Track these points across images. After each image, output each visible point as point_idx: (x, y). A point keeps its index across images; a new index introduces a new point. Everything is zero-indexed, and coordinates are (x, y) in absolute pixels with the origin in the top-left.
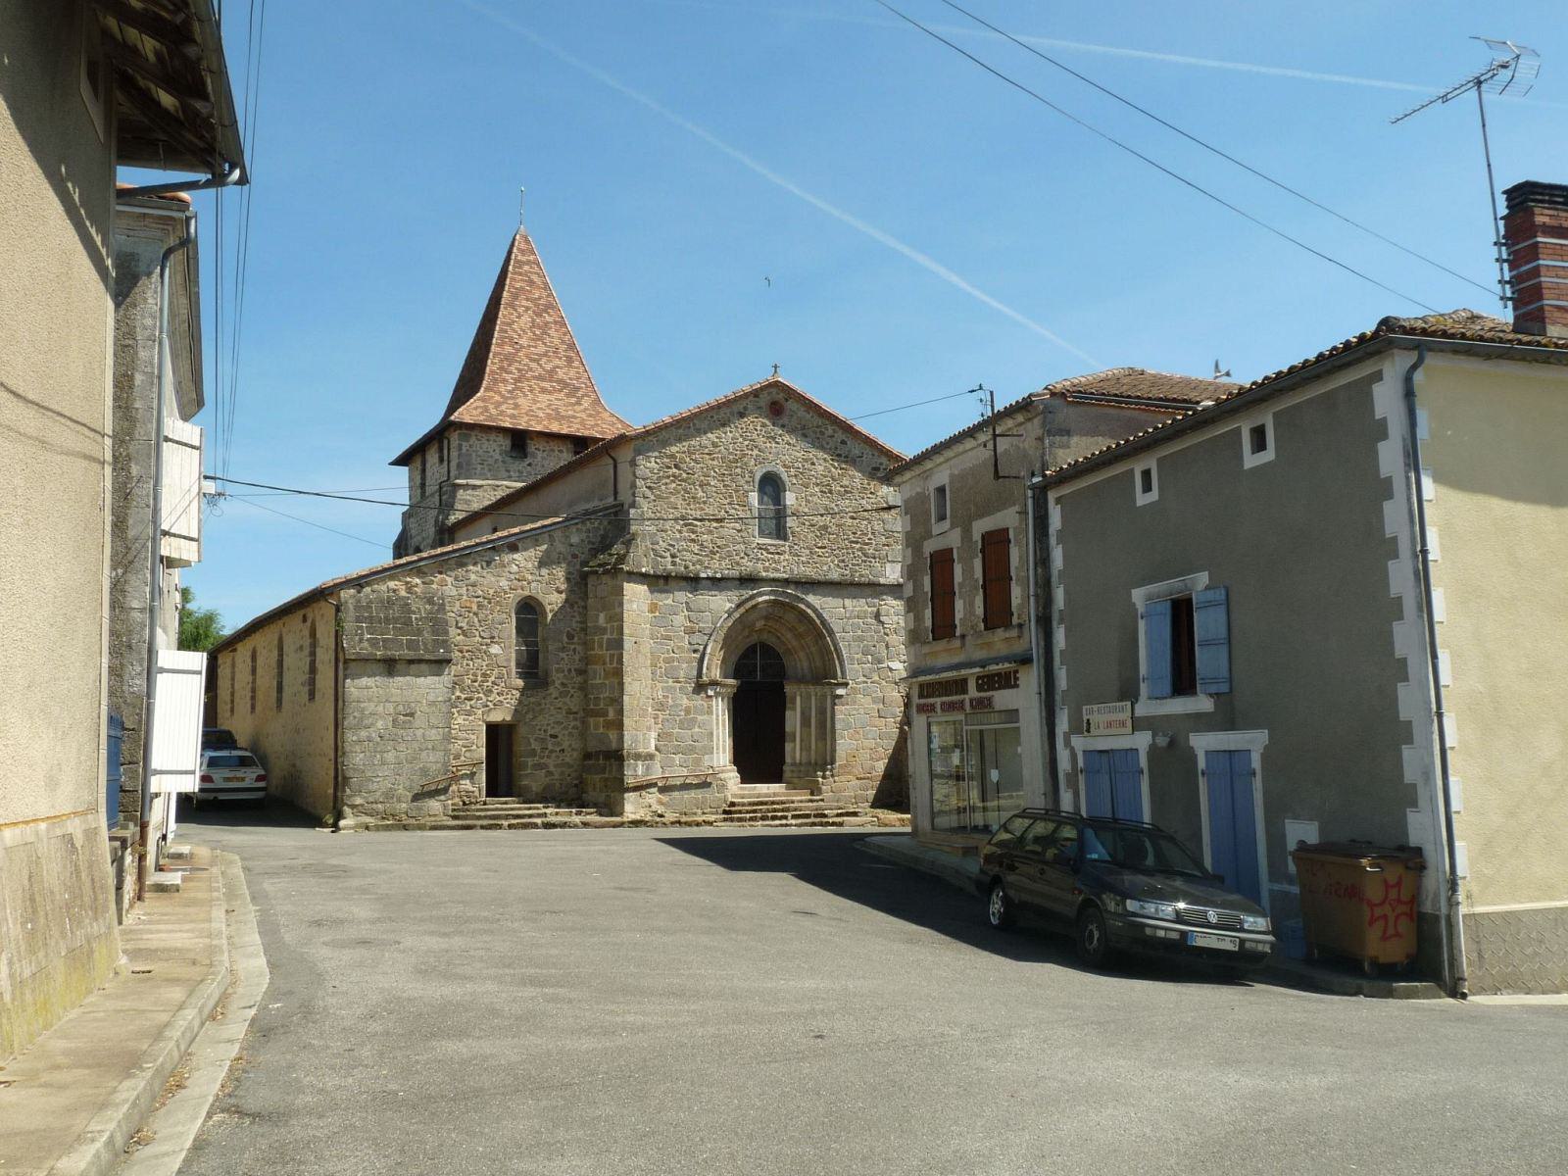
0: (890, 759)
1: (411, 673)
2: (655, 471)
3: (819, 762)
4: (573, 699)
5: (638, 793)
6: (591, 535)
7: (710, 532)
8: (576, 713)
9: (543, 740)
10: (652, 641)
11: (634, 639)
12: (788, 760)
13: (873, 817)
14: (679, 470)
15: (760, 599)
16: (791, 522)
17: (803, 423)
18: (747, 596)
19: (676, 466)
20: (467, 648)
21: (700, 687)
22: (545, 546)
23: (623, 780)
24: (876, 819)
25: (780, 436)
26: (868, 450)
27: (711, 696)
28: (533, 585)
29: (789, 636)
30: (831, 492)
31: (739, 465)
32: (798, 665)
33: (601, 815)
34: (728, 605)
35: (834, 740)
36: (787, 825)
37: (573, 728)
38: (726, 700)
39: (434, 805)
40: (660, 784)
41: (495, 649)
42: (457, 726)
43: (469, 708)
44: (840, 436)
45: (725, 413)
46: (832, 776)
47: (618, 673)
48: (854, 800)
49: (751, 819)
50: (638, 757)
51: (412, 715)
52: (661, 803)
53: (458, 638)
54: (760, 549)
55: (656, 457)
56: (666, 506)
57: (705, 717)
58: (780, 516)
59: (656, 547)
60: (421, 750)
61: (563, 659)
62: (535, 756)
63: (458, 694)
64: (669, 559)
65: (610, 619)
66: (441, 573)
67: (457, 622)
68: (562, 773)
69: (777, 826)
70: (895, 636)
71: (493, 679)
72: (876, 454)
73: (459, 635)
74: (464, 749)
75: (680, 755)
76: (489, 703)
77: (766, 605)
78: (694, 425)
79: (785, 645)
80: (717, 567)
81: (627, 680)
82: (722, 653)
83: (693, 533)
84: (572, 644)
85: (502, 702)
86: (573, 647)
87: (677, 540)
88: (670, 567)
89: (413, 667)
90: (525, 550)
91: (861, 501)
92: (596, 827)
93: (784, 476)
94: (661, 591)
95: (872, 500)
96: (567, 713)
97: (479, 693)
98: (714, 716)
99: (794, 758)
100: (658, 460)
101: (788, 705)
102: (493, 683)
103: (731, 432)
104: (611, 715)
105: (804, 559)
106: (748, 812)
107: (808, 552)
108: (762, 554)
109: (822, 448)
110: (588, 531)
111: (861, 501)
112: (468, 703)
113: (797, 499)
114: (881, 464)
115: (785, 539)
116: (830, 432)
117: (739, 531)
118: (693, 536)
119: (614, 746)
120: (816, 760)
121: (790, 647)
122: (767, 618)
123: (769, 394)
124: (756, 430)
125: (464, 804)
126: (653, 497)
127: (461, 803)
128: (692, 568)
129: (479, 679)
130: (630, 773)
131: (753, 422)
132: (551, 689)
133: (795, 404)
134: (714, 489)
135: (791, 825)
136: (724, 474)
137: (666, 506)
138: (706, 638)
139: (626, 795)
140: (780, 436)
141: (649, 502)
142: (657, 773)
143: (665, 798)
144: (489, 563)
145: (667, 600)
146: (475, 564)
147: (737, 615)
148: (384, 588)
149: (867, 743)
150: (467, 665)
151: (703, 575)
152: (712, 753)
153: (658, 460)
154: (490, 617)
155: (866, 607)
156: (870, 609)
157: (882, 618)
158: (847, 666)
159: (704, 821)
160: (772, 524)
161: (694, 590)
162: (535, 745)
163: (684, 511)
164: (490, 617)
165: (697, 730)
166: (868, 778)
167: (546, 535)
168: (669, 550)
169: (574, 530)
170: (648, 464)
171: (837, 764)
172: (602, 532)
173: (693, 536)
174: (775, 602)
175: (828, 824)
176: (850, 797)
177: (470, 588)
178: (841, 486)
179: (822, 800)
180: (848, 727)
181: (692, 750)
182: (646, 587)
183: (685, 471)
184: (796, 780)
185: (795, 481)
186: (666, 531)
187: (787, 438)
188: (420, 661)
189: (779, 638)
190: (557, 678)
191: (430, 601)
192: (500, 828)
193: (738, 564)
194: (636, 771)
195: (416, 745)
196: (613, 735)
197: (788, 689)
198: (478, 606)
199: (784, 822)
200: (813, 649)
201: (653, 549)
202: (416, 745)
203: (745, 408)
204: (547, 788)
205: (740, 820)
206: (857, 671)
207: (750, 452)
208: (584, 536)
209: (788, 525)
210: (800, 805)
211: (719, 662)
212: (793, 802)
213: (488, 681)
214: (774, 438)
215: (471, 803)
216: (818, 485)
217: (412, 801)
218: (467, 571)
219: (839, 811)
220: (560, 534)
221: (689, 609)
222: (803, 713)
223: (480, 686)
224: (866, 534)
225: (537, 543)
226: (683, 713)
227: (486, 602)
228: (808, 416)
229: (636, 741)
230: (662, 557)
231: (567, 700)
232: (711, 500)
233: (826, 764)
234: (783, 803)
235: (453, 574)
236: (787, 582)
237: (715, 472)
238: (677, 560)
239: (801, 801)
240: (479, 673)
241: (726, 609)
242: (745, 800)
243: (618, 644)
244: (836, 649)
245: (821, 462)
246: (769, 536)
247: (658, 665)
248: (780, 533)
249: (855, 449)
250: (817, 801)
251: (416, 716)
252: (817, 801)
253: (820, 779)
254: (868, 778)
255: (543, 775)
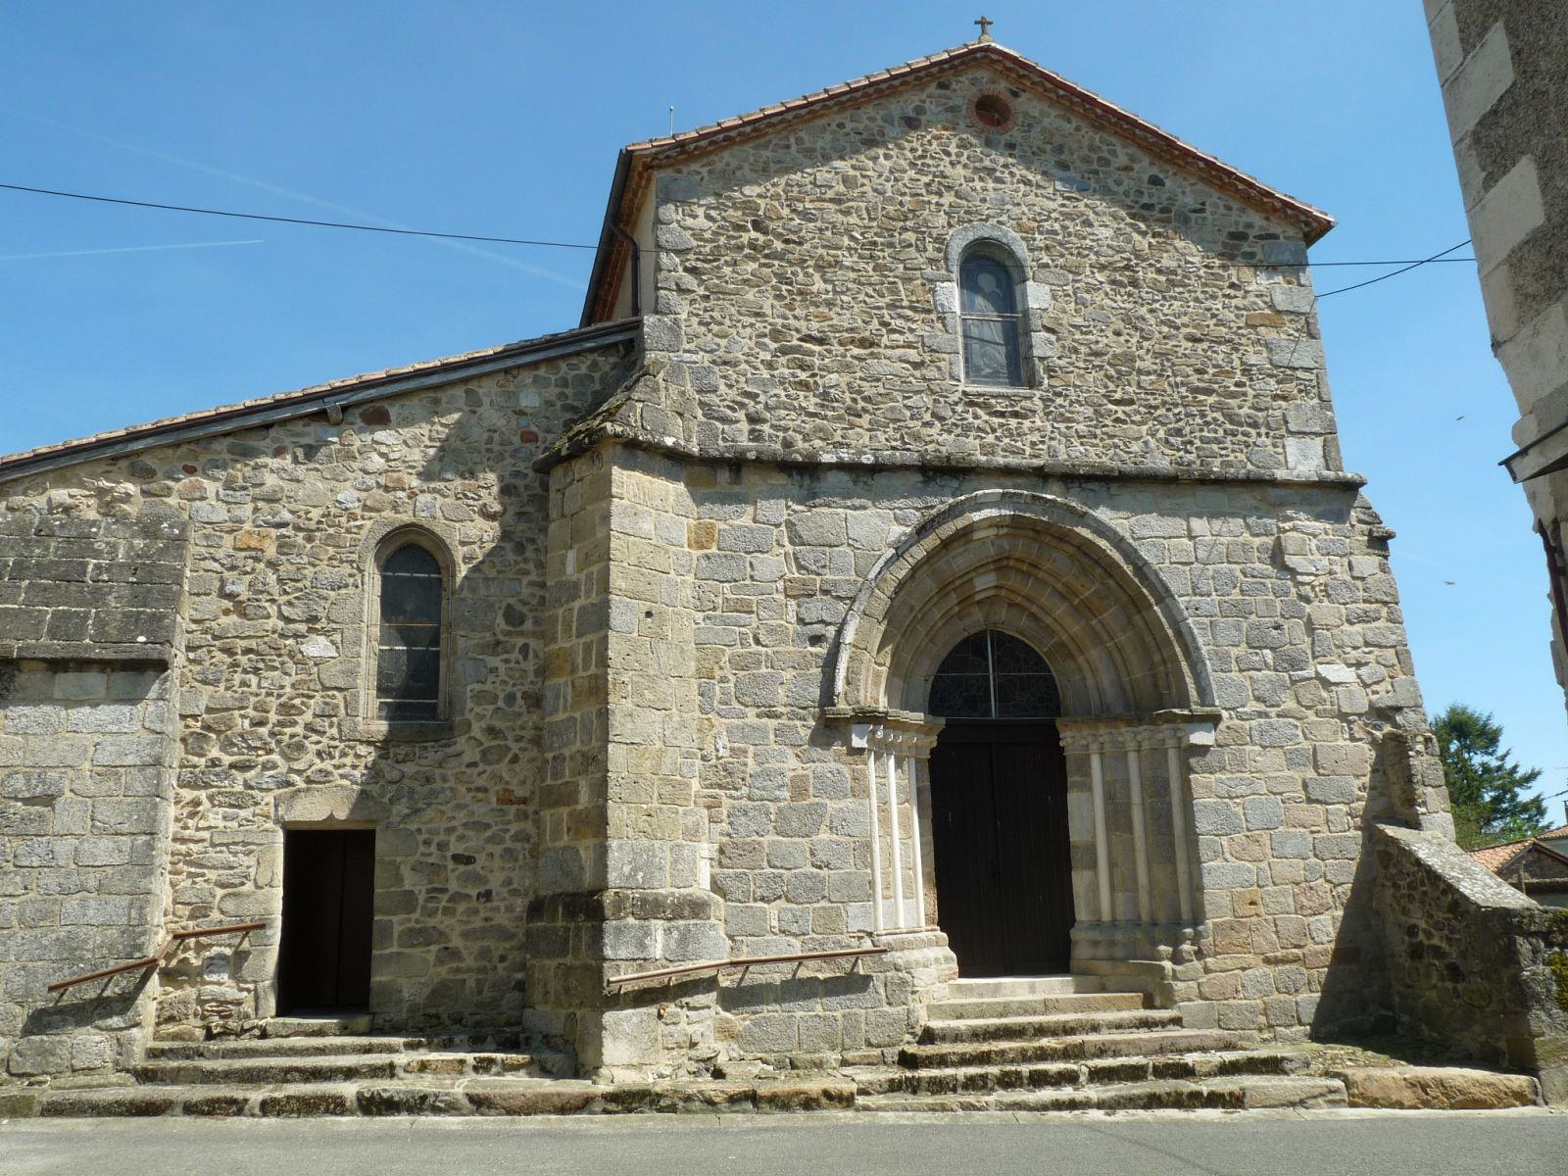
0: (1347, 908)
1: (58, 694)
2: (708, 235)
3: (1162, 918)
4: (517, 767)
5: (653, 1010)
6: (569, 391)
7: (847, 368)
8: (524, 801)
9: (435, 869)
10: (700, 616)
11: (645, 606)
12: (1082, 914)
13: (1327, 1074)
14: (765, 232)
15: (977, 516)
16: (1041, 344)
17: (1057, 140)
18: (943, 508)
19: (757, 226)
20: (244, 643)
21: (831, 728)
22: (456, 416)
23: (600, 971)
24: (1338, 1083)
25: (1006, 166)
26: (1214, 198)
27: (860, 751)
28: (423, 499)
29: (1060, 610)
30: (1134, 283)
31: (909, 224)
32: (1090, 681)
33: (546, 1072)
34: (897, 531)
35: (1195, 860)
36: (1072, 1105)
37: (516, 838)
38: (910, 766)
39: (91, 1042)
40: (725, 982)
41: (317, 647)
42: (206, 835)
43: (239, 788)
44: (1145, 167)
45: (872, 119)
46: (1200, 954)
47: (598, 690)
48: (1262, 1019)
49: (971, 1083)
50: (651, 908)
51: (49, 800)
52: (727, 1033)
53: (224, 620)
54: (972, 404)
55: (709, 207)
56: (733, 310)
57: (849, 802)
58: (1016, 332)
59: (713, 398)
60: (66, 892)
61: (494, 670)
62: (413, 911)
63: (214, 752)
64: (745, 426)
65: (585, 561)
66: (190, 471)
67: (223, 582)
68: (484, 954)
69: (1044, 1107)
70: (1326, 602)
71: (308, 717)
72: (1235, 205)
73: (226, 612)
74: (220, 892)
75: (782, 903)
76: (294, 777)
77: (992, 532)
78: (799, 141)
79: (1053, 633)
80: (865, 443)
81: (620, 705)
82: (887, 658)
83: (802, 368)
84: (522, 634)
85: (327, 773)
86: (520, 641)
87: (763, 383)
88: (744, 442)
89: (66, 681)
90: (408, 422)
91: (1208, 304)
92: (510, 1112)
93: (1021, 249)
94: (725, 499)
95: (1234, 302)
96: (500, 801)
97: (270, 752)
98: (874, 801)
99: (1096, 909)
100: (713, 213)
101: (1073, 778)
102: (309, 727)
103: (887, 157)
104: (584, 798)
105: (1081, 427)
106: (965, 1060)
107: (1089, 411)
108: (976, 417)
109: (1106, 193)
110: (565, 383)
111: (1208, 304)
112: (239, 776)
113: (1054, 298)
114: (1249, 226)
115: (1033, 383)
116: (1122, 159)
117: (917, 365)
118: (803, 376)
119: (588, 879)
120: (1152, 913)
121: (1065, 637)
122: (1000, 564)
123: (974, 82)
124: (948, 154)
125: (210, 1036)
126: (701, 291)
127: (200, 1033)
128: (800, 444)
129: (273, 717)
130: (623, 953)
131: (936, 138)
132: (461, 743)
133: (1035, 103)
134: (852, 275)
135: (1086, 1105)
136: (875, 243)
137: (733, 310)
138: (842, 607)
139: (609, 1017)
140: (1006, 166)
141: (693, 302)
142: (713, 949)
143: (739, 1020)
144: (310, 452)
145: (741, 518)
146: (278, 452)
147: (919, 552)
148: (39, 501)
149: (1281, 867)
150: (244, 684)
151: (827, 458)
152: (871, 897)
153: (713, 213)
154: (309, 572)
155: (1247, 535)
156: (1257, 541)
157: (1291, 561)
158: (1214, 677)
159: (826, 1094)
160: (1000, 354)
161: (809, 497)
162: (411, 881)
163: (780, 321)
164: (309, 572)
165: (824, 835)
166: (1296, 960)
167: (459, 392)
168: (742, 405)
169: (529, 381)
170: (689, 222)
171: (1209, 923)
172: (597, 387)
173: (803, 376)
174: (1016, 523)
175: (1195, 1100)
176: (1252, 1010)
177: (260, 504)
178: (1159, 271)
179: (1177, 1021)
180: (1228, 828)
181: (814, 889)
182: (681, 487)
183: (779, 236)
184: (1104, 967)
185: (1046, 259)
186: (734, 364)
187: (1020, 171)
188: (83, 664)
189: (1034, 617)
190: (477, 717)
191: (149, 530)
192: (239, 1112)
193: (917, 437)
194: (642, 946)
195: (51, 880)
196: (586, 854)
197: (1071, 739)
198: (280, 546)
199: (1067, 1092)
200: (1121, 638)
201: (701, 404)
202: (51, 880)
203: (919, 110)
204: (440, 991)
205: (938, 1086)
206: (1240, 687)
207: (934, 199)
208: (552, 392)
209: (1036, 352)
210: (1117, 1036)
211: (885, 669)
212: (1095, 1028)
213: (294, 724)
214: (991, 171)
215: (226, 1033)
216: (1102, 268)
217: (27, 1031)
218: (256, 468)
219: (1229, 1056)
220: (495, 389)
221: (796, 539)
222: (1109, 797)
223: (272, 734)
224: (1230, 374)
225: (436, 410)
226: (786, 794)
227: (300, 538)
228: (1069, 128)
229: (649, 863)
230: (724, 420)
231: (503, 768)
232: (845, 298)
233: (1177, 923)
234: (1068, 1030)
235: (221, 474)
236: (1041, 475)
237: (853, 238)
238: (766, 428)
239: (1119, 1026)
240: (273, 703)
241: (892, 538)
242: (962, 1024)
243: (599, 618)
244: (1179, 634)
245: (1106, 219)
246: (993, 377)
247: (718, 673)
248: (1019, 367)
249: (1184, 192)
250: (1163, 1024)
251: (59, 803)
252: (1163, 1024)
253: (1168, 965)
254: (1296, 960)
255: (431, 958)
